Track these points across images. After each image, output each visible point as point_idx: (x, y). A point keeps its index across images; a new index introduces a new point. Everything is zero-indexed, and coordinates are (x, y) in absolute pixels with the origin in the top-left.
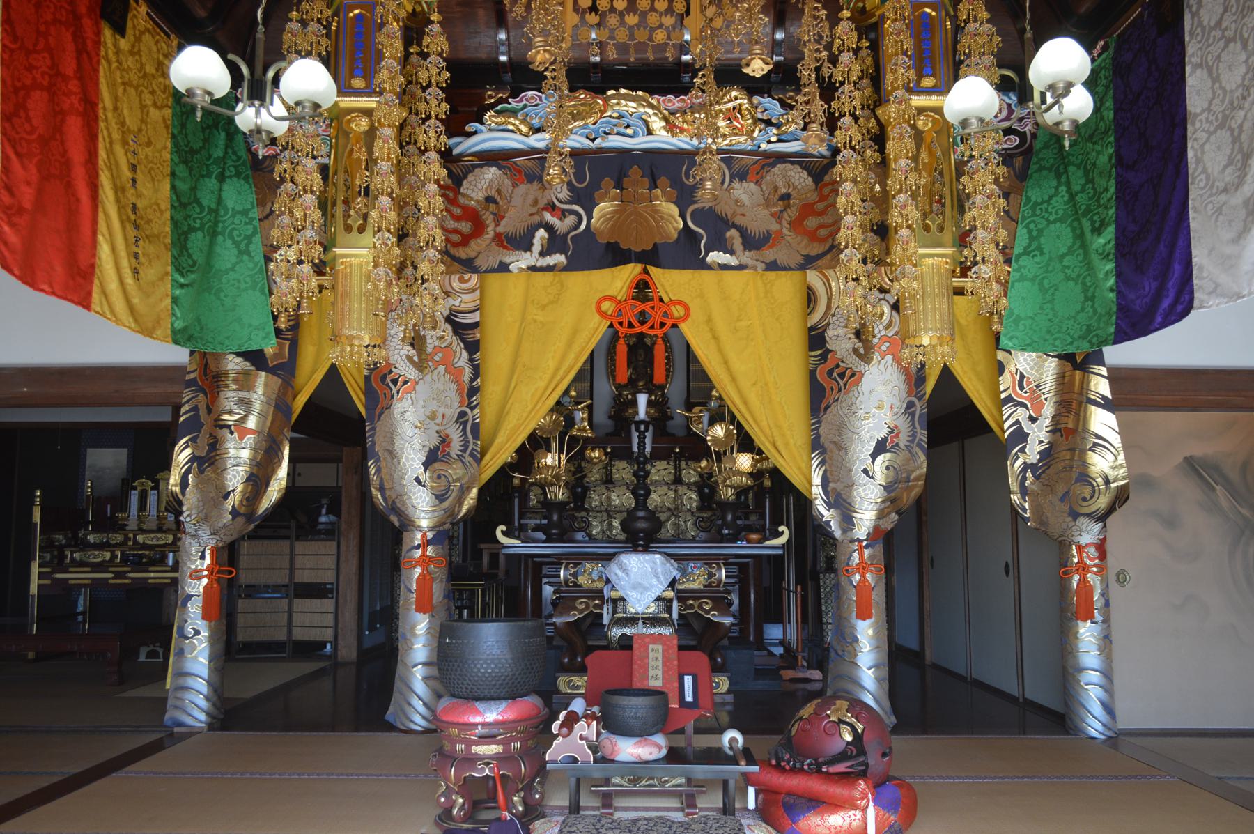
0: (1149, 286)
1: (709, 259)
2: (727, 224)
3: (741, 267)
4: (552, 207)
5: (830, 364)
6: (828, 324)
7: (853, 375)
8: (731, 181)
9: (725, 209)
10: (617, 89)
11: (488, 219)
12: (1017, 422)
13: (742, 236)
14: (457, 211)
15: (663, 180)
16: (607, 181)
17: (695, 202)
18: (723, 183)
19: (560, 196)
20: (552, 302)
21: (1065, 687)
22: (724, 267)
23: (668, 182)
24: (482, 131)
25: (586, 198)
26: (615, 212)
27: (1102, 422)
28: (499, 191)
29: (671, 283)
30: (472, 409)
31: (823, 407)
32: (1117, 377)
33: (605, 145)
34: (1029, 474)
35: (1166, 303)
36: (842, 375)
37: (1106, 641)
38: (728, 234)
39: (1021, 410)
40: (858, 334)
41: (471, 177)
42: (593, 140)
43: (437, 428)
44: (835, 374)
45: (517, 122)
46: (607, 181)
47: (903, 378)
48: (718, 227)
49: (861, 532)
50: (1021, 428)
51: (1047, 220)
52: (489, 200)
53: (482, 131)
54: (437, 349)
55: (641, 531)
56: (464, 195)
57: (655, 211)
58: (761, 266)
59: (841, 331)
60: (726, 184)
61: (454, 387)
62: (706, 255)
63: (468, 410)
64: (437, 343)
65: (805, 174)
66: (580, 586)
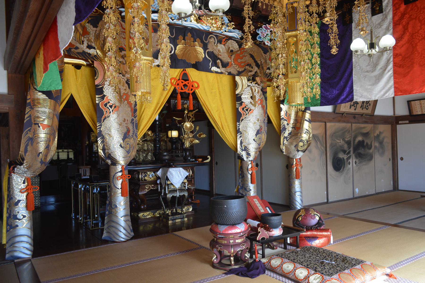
0: (335, 92)
1: (212, 69)
3: (221, 73)
5: (243, 106)
6: (242, 94)
7: (250, 110)
9: (216, 53)
12: (284, 125)
13: (221, 62)
16: (181, 37)
17: (208, 49)
18: (215, 43)
20: (155, 78)
21: (290, 198)
22: (217, 72)
23: (200, 40)
26: (183, 48)
27: (306, 125)
29: (194, 74)
30: (135, 117)
31: (241, 120)
32: (313, 114)
34: (285, 139)
35: (342, 97)
36: (247, 110)
37: (301, 184)
38: (218, 61)
39: (285, 121)
40: (251, 97)
42: (173, 20)
43: (126, 125)
44: (245, 109)
46: (181, 37)
47: (263, 112)
48: (214, 58)
49: (251, 158)
50: (285, 127)
54: (124, 94)
55: (167, 159)
57: (196, 51)
58: (227, 73)
59: (246, 96)
61: (130, 109)
62: (211, 68)
63: (134, 118)
64: (124, 92)
65: (237, 44)
66: (146, 180)
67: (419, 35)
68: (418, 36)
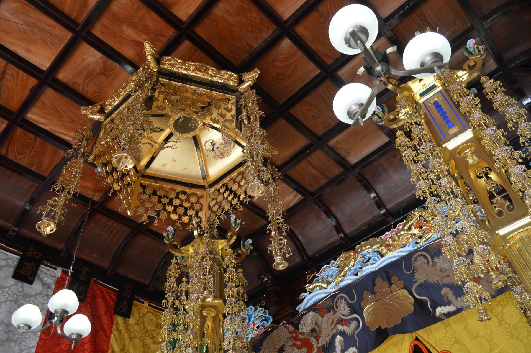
1: (437, 314)
2: (438, 287)
3: (459, 311)
4: (341, 322)
8: (432, 260)
10: (359, 244)
11: (313, 340)
13: (451, 290)
14: (299, 343)
15: (394, 279)
17: (416, 282)
19: (344, 313)
22: (449, 315)
24: (306, 296)
25: (356, 309)
28: (316, 324)
33: (363, 274)
38: (442, 292)
41: (302, 322)
42: (357, 275)
45: (320, 284)
51: (10, 290)
52: (313, 330)
53: (306, 296)
56: (301, 333)
60: (431, 263)
62: (435, 312)
67: (7, 295)
68: (9, 295)
